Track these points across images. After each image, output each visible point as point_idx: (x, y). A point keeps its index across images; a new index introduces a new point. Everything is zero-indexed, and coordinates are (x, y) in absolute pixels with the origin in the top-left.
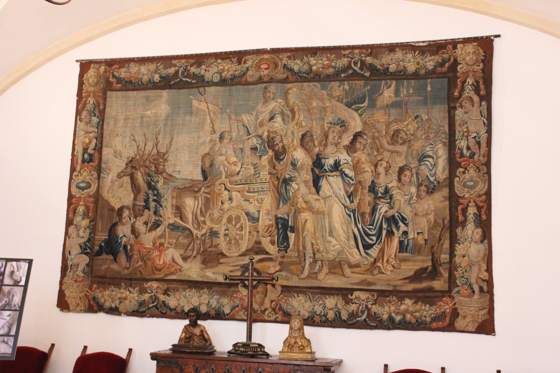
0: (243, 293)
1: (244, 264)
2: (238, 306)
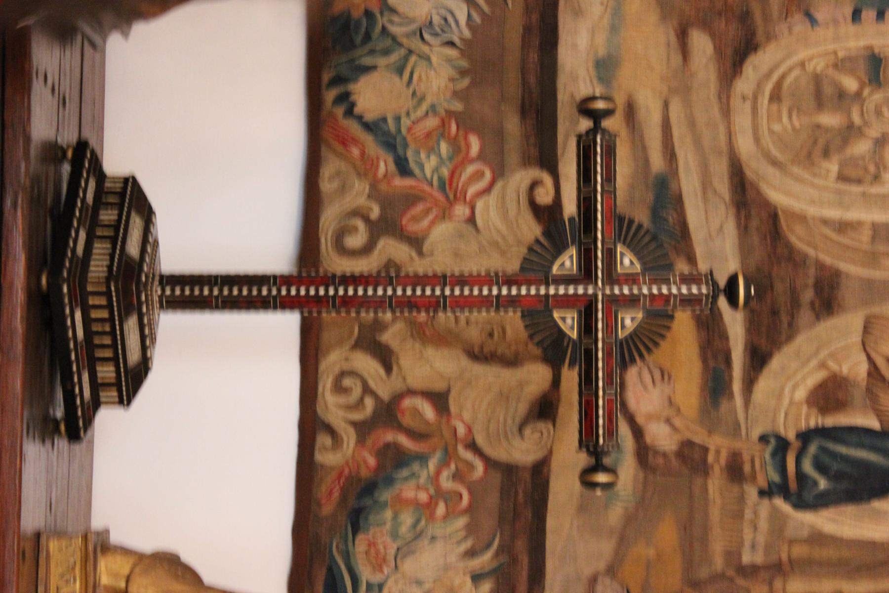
0: (492, 199)
2: (403, 168)
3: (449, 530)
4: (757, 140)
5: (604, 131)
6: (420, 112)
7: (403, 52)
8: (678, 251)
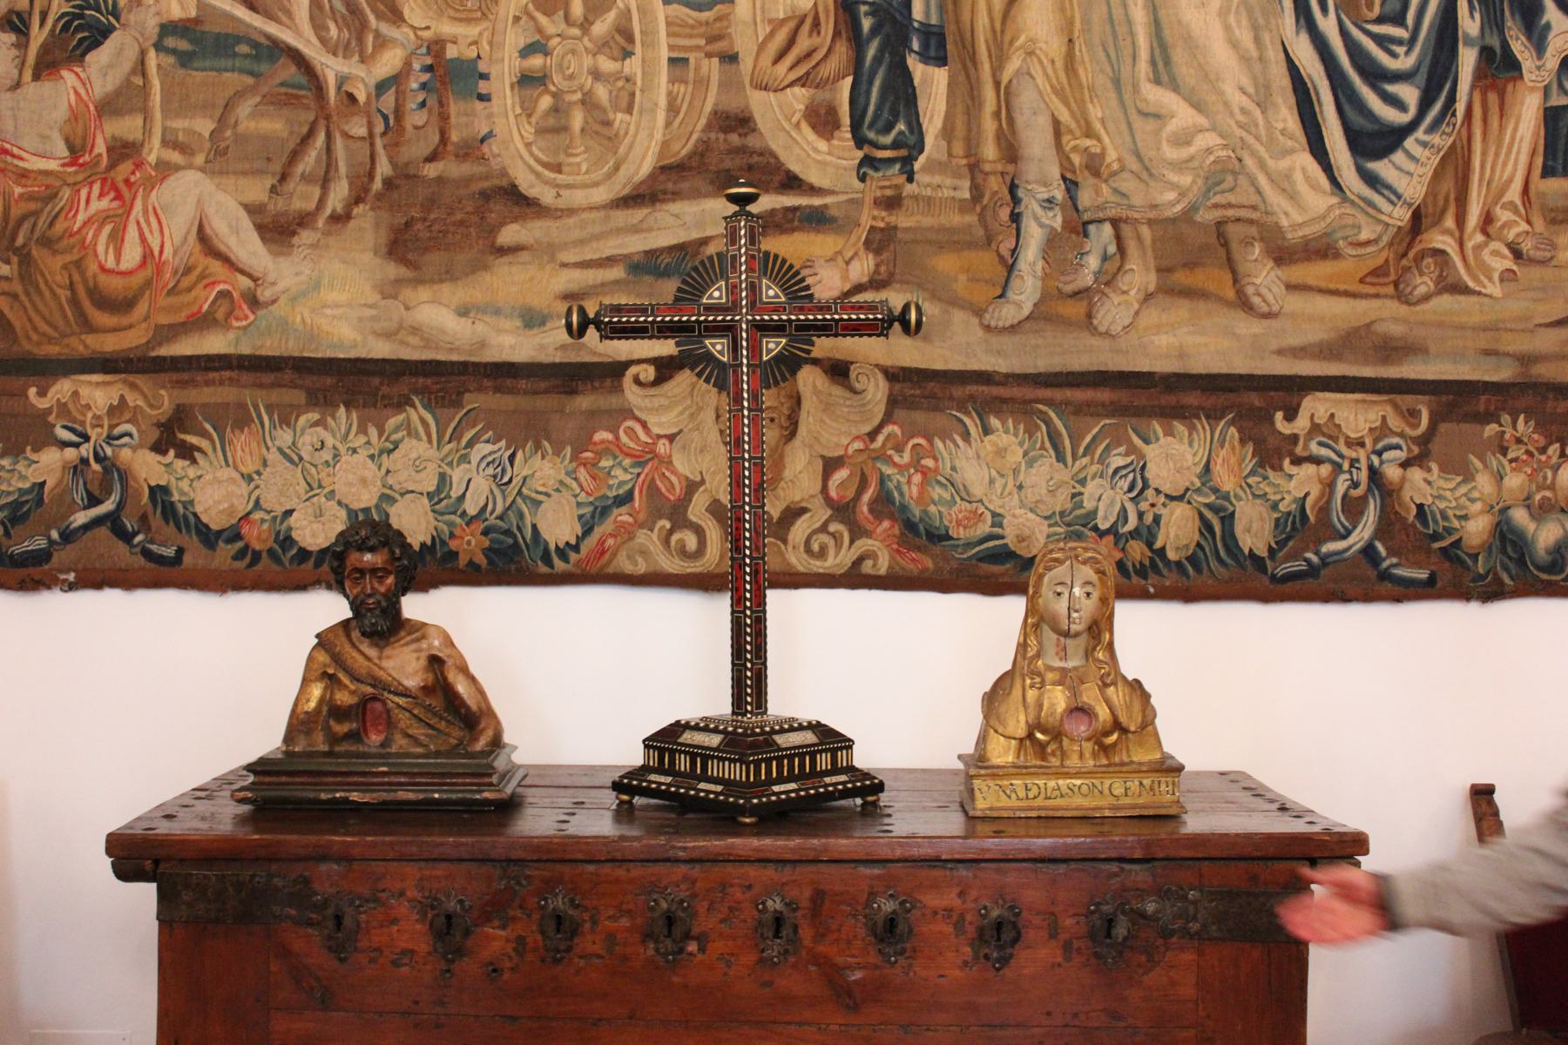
0: (651, 420)
1: (650, 253)
2: (627, 498)
3: (946, 455)
4: (596, 184)
5: (598, 314)
6: (575, 485)
7: (519, 500)
8: (697, 253)
